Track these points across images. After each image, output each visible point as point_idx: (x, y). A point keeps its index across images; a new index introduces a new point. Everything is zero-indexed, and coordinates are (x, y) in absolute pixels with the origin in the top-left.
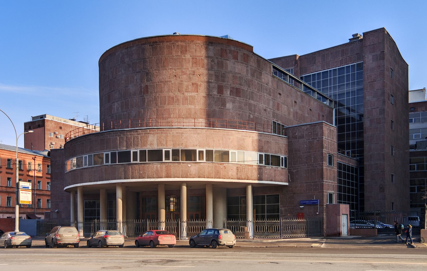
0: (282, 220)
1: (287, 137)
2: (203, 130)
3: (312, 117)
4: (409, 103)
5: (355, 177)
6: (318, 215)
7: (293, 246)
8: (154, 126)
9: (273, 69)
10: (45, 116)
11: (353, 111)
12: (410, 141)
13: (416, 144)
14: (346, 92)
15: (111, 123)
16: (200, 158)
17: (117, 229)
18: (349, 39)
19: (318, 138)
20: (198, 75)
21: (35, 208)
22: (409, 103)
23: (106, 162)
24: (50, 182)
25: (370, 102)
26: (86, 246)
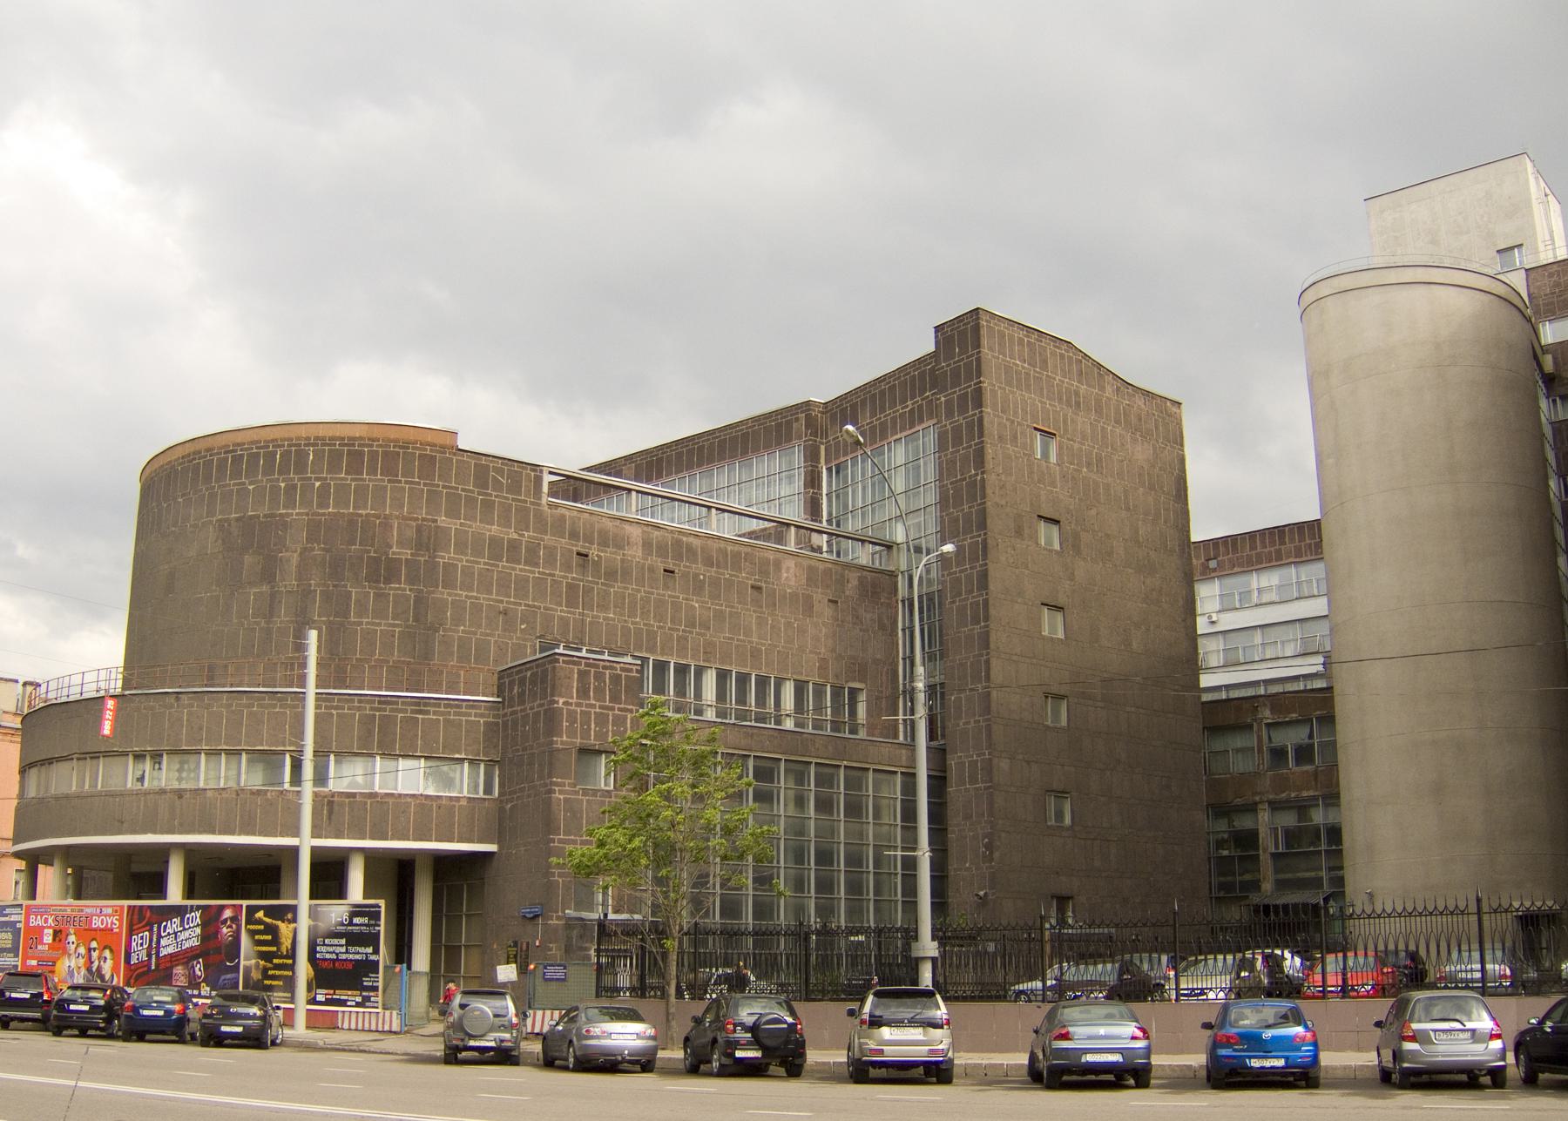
2: (149, 696)
4: (1201, 686)
8: (249, 583)
9: (284, 899)
10: (13, 845)
12: (1196, 586)
14: (882, 457)
15: (103, 781)
16: (1178, 490)
17: (666, 692)
18: (938, 329)
19: (562, 741)
20: (1159, 940)
21: (901, 515)
22: (1201, 686)
23: (485, 793)
24: (142, 785)
26: (1117, 1062)
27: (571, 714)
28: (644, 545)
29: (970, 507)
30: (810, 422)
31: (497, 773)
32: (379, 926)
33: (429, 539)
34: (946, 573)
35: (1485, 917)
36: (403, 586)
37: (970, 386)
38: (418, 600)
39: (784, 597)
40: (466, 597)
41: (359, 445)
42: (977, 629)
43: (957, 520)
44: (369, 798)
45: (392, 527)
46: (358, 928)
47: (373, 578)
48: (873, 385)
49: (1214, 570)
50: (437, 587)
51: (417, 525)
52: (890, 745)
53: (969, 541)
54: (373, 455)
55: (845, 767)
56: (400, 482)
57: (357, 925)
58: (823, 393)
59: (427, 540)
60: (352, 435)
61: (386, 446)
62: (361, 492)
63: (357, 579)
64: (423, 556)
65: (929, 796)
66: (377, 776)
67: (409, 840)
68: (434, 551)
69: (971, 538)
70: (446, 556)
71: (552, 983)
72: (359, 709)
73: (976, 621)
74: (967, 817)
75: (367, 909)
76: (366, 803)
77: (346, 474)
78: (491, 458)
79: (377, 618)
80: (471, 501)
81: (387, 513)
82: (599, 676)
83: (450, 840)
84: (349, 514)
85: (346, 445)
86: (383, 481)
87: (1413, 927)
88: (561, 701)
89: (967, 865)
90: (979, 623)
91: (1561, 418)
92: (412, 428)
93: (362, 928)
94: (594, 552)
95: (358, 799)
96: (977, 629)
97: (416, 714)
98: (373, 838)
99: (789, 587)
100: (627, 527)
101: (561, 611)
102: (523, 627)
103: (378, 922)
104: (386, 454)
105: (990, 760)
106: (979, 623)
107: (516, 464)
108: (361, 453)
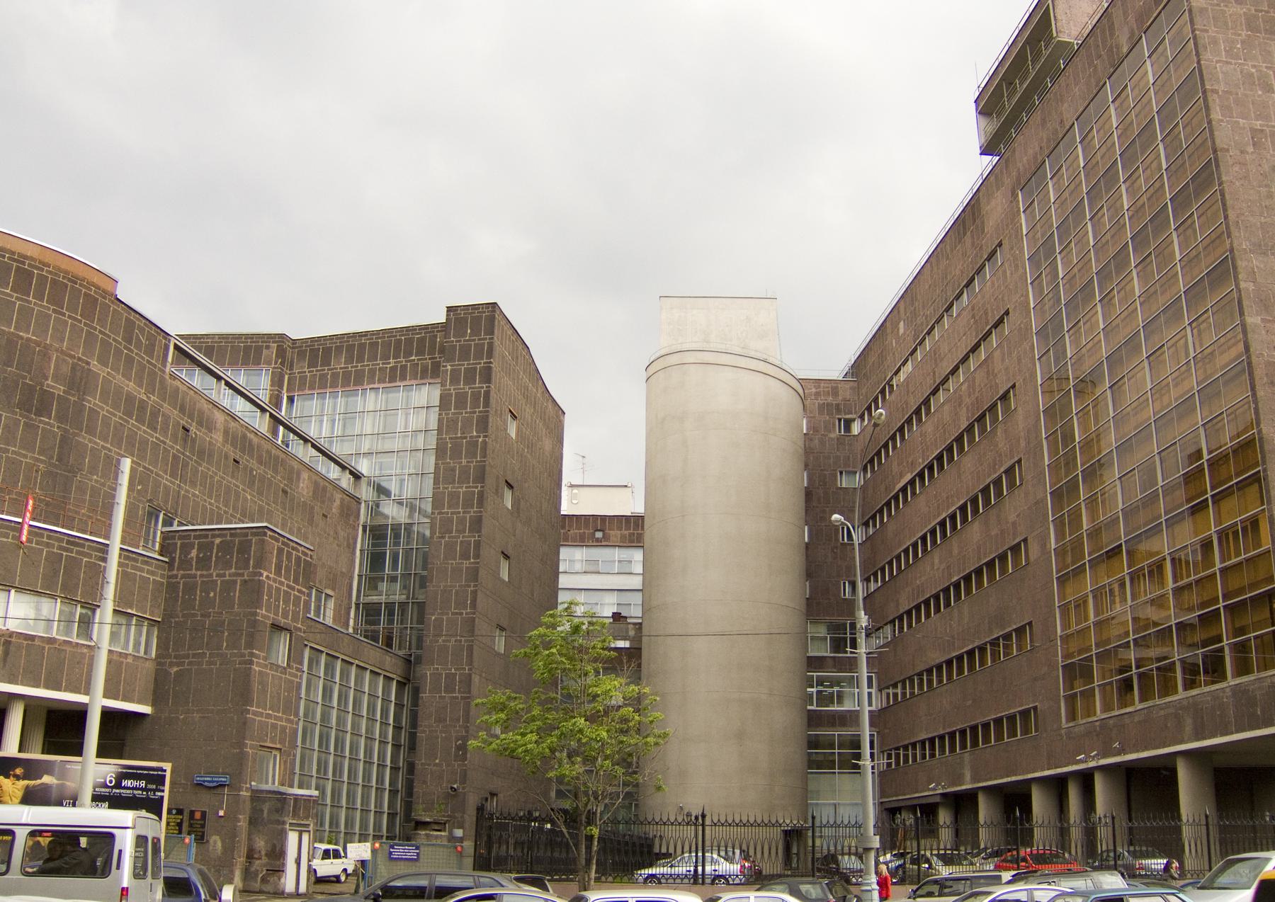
0: (1021, 825)
1: (167, 560)
3: (1254, 70)
5: (44, 522)
6: (223, 819)
7: (135, 640)
11: (1118, 388)
13: (283, 893)
18: (450, 309)
25: (401, 366)
27: (270, 587)
28: (224, 433)
29: (468, 462)
30: (281, 352)
31: (156, 633)
32: (163, 791)
33: (81, 379)
34: (436, 512)
35: (708, 830)
36: (52, 421)
37: (480, 363)
38: (64, 440)
39: (298, 503)
40: (102, 446)
41: (30, 265)
42: (466, 564)
43: (453, 470)
44: (48, 644)
45: (50, 359)
46: (128, 791)
47: (25, 406)
48: (340, 338)
49: (598, 540)
50: (81, 431)
51: (73, 363)
52: (369, 646)
53: (464, 489)
54: (42, 279)
55: (357, 665)
56: (64, 315)
57: (125, 788)
58: (298, 332)
59: (79, 381)
60: (23, 252)
61: (56, 274)
62: (25, 313)
63: (9, 403)
64: (73, 395)
65: (17, 684)
66: (57, 619)
67: (80, 693)
68: (84, 394)
69: (466, 487)
70: (93, 401)
71: (399, 863)
72: (48, 545)
73: (465, 556)
74: (440, 720)
75: (156, 773)
76: (44, 648)
77: (11, 290)
78: (137, 316)
79: (24, 448)
80: (118, 352)
81: (48, 342)
82: (289, 554)
83: (116, 698)
84: (9, 333)
85: (15, 260)
86: (49, 309)
87: (717, 835)
88: (265, 574)
89: (437, 761)
90: (468, 558)
91: (844, 486)
92: (82, 265)
93: (136, 792)
94: (193, 429)
95: (37, 642)
96: (466, 564)
97: (100, 561)
98: (47, 687)
99: (303, 496)
100: (215, 411)
101: (166, 480)
102: (139, 488)
103: (161, 788)
104: (54, 282)
105: (470, 675)
106: (468, 558)
107: (154, 328)
108: (31, 274)
